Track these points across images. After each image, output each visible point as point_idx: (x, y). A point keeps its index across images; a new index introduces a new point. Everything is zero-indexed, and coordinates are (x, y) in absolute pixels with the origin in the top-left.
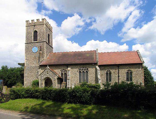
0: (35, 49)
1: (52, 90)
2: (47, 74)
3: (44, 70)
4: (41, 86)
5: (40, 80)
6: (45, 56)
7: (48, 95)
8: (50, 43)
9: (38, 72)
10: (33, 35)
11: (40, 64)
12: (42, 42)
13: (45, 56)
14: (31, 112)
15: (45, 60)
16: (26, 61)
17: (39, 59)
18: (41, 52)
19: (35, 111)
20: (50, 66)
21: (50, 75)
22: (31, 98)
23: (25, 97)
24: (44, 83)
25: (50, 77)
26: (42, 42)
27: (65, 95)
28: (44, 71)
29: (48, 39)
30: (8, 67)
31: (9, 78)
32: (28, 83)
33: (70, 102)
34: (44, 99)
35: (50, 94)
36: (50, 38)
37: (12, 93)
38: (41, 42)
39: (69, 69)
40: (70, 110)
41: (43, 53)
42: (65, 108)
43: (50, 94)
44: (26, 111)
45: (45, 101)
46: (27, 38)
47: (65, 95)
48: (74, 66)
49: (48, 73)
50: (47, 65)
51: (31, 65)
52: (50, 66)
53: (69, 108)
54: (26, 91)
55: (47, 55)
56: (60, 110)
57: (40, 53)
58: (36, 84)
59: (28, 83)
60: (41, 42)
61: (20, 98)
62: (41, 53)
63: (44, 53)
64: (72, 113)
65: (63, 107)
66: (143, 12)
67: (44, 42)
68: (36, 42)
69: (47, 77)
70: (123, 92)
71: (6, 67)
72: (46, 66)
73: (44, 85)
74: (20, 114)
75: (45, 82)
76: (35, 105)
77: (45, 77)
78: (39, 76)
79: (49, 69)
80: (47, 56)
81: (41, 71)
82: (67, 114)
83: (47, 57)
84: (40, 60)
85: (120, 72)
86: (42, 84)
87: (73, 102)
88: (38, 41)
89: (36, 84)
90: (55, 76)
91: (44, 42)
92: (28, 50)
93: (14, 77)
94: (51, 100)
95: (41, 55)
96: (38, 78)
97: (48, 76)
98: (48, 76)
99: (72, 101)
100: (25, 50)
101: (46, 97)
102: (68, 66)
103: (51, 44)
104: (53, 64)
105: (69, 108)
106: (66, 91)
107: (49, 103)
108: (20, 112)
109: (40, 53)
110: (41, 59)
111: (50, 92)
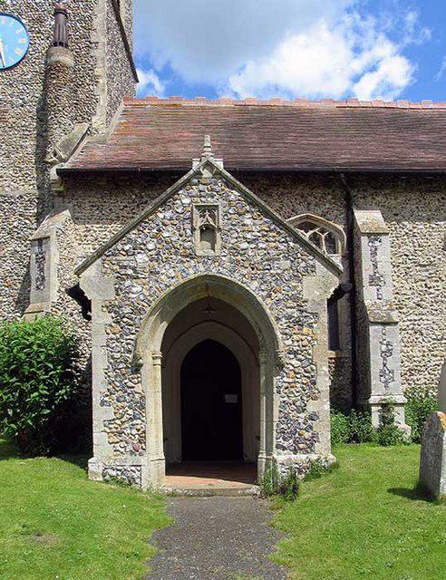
2: (202, 248)
3: (117, 228)
4: (124, 388)
6: (103, 100)
9: (40, 241)
11: (66, 166)
13: (103, 100)
21: (235, 250)
25: (236, 278)
39: (367, 218)
41: (82, 77)
48: (412, 201)
49: (208, 232)
62: (60, 67)
66: (416, 81)
69: (208, 282)
70: (375, 421)
77: (174, 275)
78: (91, 272)
85: (382, 315)
98: (222, 270)
102: (353, 193)
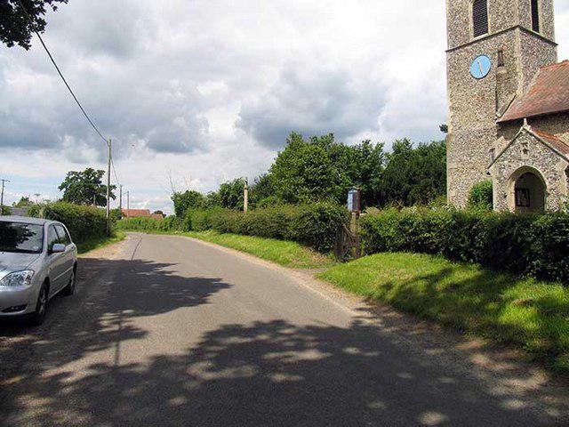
0: (482, 65)
1: (476, 221)
5: (495, 182)
6: (521, 83)
7: (463, 242)
8: (540, 24)
10: (470, 16)
11: (501, 120)
12: (506, 31)
13: (521, 83)
14: (395, 305)
15: (523, 96)
16: (452, 114)
17: (497, 99)
18: (504, 71)
19: (405, 301)
20: (533, 120)
21: (534, 156)
22: (417, 252)
23: (395, 245)
24: (510, 190)
26: (506, 31)
27: (520, 239)
28: (511, 144)
29: (530, 14)
30: (411, 142)
31: (412, 182)
32: (457, 196)
33: (544, 276)
34: (453, 256)
35: (471, 237)
36: (539, 6)
37: (365, 232)
38: (502, 32)
40: (531, 311)
41: (512, 73)
42: (512, 299)
43: (471, 237)
44: (381, 298)
45: (454, 266)
46: (452, 30)
47: (520, 239)
49: (525, 151)
50: (522, 119)
51: (469, 126)
52: (533, 120)
53: (527, 304)
54: (401, 223)
55: (528, 78)
56: (492, 306)
57: (498, 77)
58: (484, 195)
59: (457, 196)
60: (502, 32)
61: (384, 249)
63: (516, 74)
64: (532, 326)
65: (508, 293)
67: (513, 28)
68: (483, 39)
71: (407, 143)
72: (519, 122)
73: (510, 204)
74: (363, 305)
75: (516, 189)
76: (416, 279)
77: (515, 167)
79: (531, 134)
80: (527, 84)
81: (501, 143)
82: (507, 328)
83: (531, 84)
84: (502, 104)
86: (505, 197)
87: (556, 276)
88: (490, 33)
89: (484, 195)
90: (558, 161)
91: (513, 28)
92: (456, 74)
93: (427, 175)
94: (475, 262)
95: (502, 80)
96: (488, 174)
97: (526, 161)
99: (552, 271)
100: (448, 74)
101: (460, 249)
103: (545, 31)
104: (551, 111)
105: (527, 304)
106: (527, 226)
107: (463, 274)
108: (365, 301)
109: (498, 77)
110: (506, 99)
111: (471, 227)
